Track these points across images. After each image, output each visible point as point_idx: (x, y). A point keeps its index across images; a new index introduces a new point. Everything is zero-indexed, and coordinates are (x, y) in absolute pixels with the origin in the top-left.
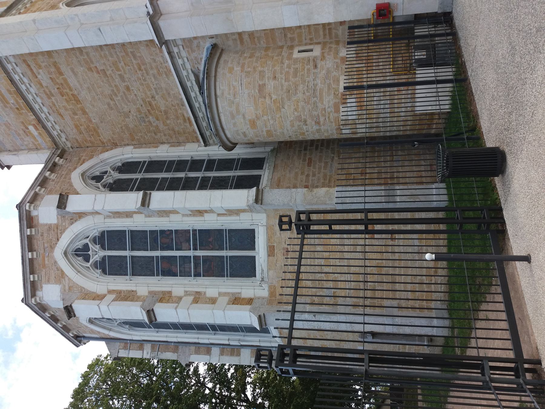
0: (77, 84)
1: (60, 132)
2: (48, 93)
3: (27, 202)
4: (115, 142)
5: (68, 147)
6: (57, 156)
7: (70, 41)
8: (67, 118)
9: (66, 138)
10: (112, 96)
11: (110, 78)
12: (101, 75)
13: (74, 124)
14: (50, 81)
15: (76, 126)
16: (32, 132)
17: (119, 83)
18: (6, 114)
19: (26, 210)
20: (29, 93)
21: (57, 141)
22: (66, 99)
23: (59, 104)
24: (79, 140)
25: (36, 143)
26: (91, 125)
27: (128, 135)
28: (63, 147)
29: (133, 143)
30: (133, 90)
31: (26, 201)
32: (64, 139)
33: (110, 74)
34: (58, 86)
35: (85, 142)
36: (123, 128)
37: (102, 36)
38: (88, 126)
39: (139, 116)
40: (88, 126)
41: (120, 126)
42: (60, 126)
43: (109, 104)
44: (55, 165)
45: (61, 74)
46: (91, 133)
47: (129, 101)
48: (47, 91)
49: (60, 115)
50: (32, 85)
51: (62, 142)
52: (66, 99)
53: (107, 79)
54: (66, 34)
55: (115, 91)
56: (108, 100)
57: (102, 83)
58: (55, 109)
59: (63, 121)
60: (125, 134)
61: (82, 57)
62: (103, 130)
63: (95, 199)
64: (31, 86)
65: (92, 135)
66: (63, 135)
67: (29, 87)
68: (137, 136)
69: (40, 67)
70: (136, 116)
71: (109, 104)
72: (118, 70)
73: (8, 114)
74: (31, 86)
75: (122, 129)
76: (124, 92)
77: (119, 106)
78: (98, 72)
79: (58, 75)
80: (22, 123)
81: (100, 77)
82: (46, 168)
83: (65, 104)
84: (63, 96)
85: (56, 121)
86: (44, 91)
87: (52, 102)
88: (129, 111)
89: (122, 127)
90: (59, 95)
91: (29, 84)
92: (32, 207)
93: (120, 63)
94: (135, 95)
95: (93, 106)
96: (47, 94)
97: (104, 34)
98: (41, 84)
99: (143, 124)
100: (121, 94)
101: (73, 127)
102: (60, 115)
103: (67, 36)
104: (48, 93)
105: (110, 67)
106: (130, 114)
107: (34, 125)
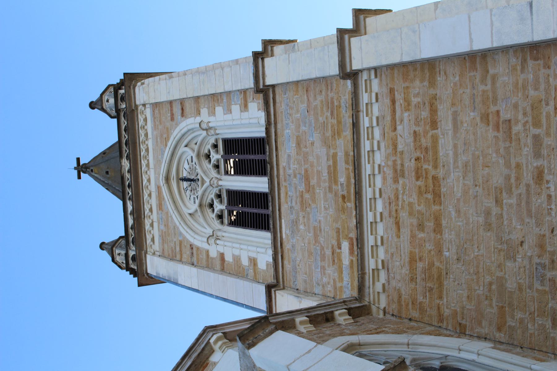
0: (451, 153)
1: (380, 267)
2: (399, 167)
3: (222, 331)
4: (463, 322)
5: (378, 308)
6: (346, 307)
7: (470, 34)
8: (406, 233)
9: (384, 285)
10: (501, 192)
11: (513, 144)
12: (500, 135)
13: (411, 252)
14: (412, 139)
15: (412, 260)
16: (343, 256)
17: (527, 159)
18: (324, 207)
19: (208, 342)
20: (371, 162)
21: (367, 284)
22: (420, 187)
23: (405, 197)
24: (403, 297)
25: (339, 285)
26: (437, 264)
27: (496, 308)
28: (369, 302)
29: (498, 335)
30: (548, 182)
31: (224, 329)
32: (379, 287)
33: (517, 134)
34: (418, 154)
35: (410, 306)
36: (494, 287)
37: (529, 22)
38: (431, 265)
39: (536, 260)
40: (431, 265)
41: (488, 279)
42: (386, 252)
43: (488, 213)
44: (328, 318)
45: (434, 124)
46: (429, 285)
47: (529, 211)
48: (399, 162)
49: (397, 224)
50: (382, 145)
51: (374, 292)
52: (420, 187)
53: (508, 144)
54: (469, 17)
55: (513, 180)
56: (490, 203)
57: (494, 155)
58: (394, 209)
59: (396, 239)
60: (491, 305)
61: (482, 87)
62: (454, 282)
63: (309, 351)
64: (379, 148)
65: (431, 290)
66: (383, 275)
67: (376, 148)
68: (513, 317)
69: (408, 106)
70: (531, 258)
71: (488, 213)
72: (537, 123)
73: (327, 206)
74: (379, 148)
75: (490, 290)
76: (528, 186)
77: (505, 223)
78: (497, 127)
79: (428, 127)
80: (338, 231)
81: (496, 137)
82: (308, 312)
83: (414, 199)
84: (418, 178)
85: (385, 239)
86: (395, 161)
87: (397, 189)
88: (520, 240)
89: (490, 284)
90: (413, 174)
91: (378, 142)
92: (220, 343)
93: (547, 104)
94: (549, 196)
95: (458, 211)
96: (395, 171)
97: (534, 17)
98: (395, 146)
99: (537, 285)
100: (522, 189)
101: (407, 259)
102: (397, 224)
103: (470, 21)
104: (399, 167)
105: (525, 114)
106: (520, 249)
107: (351, 245)
